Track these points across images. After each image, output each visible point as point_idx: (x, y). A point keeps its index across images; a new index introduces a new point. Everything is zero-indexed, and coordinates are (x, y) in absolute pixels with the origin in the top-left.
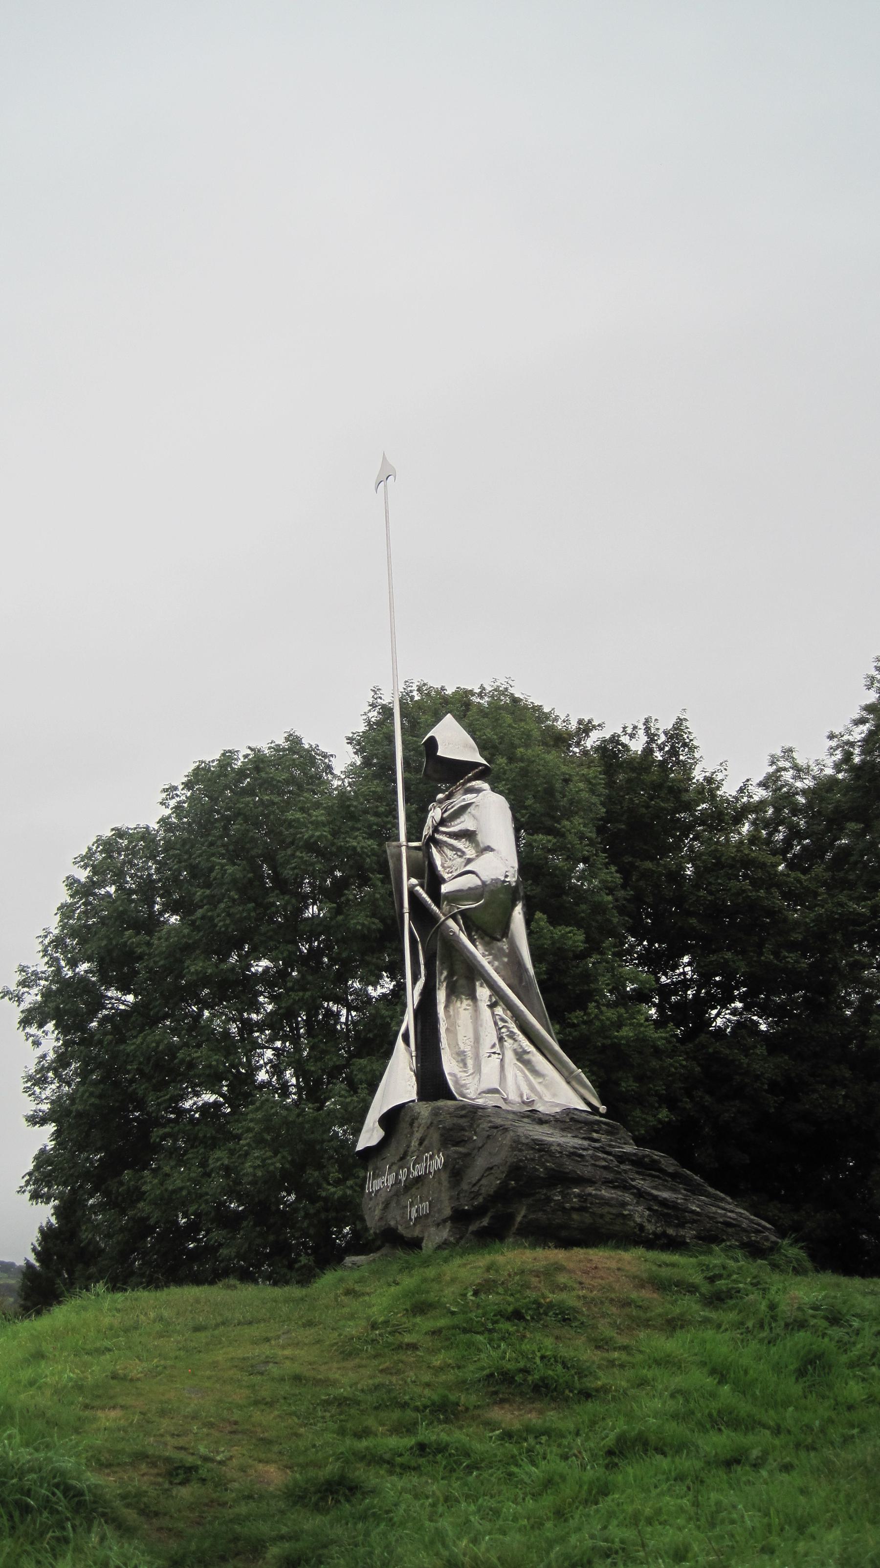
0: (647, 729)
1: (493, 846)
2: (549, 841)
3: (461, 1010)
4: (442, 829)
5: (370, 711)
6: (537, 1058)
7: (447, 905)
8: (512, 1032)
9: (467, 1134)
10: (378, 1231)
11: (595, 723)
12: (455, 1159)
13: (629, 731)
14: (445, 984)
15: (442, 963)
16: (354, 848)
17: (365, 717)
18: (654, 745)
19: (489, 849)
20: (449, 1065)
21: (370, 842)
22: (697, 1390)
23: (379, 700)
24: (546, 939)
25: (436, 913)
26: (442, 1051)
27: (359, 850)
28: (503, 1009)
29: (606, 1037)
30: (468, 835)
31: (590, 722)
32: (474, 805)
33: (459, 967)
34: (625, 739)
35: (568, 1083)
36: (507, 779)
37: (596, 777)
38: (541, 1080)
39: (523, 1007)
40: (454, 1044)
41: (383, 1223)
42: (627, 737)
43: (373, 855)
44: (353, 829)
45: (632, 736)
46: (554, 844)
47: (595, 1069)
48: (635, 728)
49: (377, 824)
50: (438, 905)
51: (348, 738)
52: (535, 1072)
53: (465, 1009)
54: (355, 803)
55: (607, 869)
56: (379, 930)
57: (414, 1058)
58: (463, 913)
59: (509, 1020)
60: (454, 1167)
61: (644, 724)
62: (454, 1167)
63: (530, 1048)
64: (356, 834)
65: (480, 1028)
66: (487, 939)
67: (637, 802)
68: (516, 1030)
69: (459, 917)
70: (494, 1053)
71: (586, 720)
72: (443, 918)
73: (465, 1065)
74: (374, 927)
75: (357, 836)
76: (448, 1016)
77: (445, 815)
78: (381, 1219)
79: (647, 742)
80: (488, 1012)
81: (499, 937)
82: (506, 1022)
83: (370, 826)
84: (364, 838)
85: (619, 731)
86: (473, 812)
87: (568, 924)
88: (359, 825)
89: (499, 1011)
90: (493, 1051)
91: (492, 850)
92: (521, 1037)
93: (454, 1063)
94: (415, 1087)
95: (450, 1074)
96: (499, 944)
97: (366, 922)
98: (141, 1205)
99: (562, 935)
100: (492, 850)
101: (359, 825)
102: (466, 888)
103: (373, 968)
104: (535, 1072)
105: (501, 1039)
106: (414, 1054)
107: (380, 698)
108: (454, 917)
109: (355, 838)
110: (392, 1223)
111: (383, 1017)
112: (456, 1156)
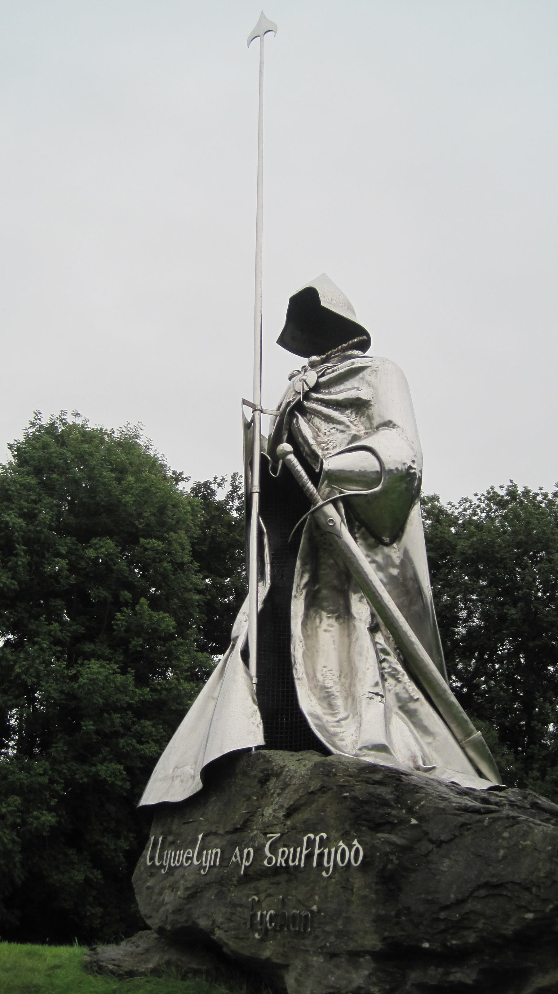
0: (233, 482)
1: (395, 420)
2: (159, 546)
4: (314, 395)
5: (30, 428)
6: (425, 709)
7: (328, 486)
8: (395, 669)
9: (394, 812)
10: (168, 927)
11: (184, 476)
12: (387, 854)
13: (219, 481)
14: (304, 592)
15: (303, 565)
16: (7, 523)
17: (26, 431)
18: (235, 495)
19: (388, 424)
20: (308, 703)
21: (20, 520)
23: (38, 421)
24: (146, 620)
25: (312, 495)
26: (297, 683)
27: (11, 524)
29: (179, 704)
30: (358, 406)
31: (181, 474)
32: (368, 370)
33: (328, 574)
34: (214, 487)
35: (463, 748)
36: (132, 494)
37: (197, 506)
38: (430, 740)
39: (414, 638)
40: (312, 676)
41: (182, 918)
42: (216, 485)
43: (21, 531)
44: (7, 507)
45: (220, 485)
46: (162, 548)
47: (166, 726)
48: (223, 479)
49: (27, 508)
50: (316, 483)
51: (9, 445)
52: (424, 730)
53: (325, 631)
54: (13, 488)
55: (196, 575)
56: (15, 590)
58: (346, 500)
59: (392, 653)
60: (385, 867)
61: (232, 477)
62: (385, 867)
63: (417, 694)
64: (10, 512)
65: (356, 658)
66: (372, 540)
67: (220, 532)
68: (399, 667)
69: (341, 505)
70: (377, 694)
71: (178, 472)
72: (321, 503)
73: (331, 706)
74: (13, 587)
75: (11, 514)
76: (306, 636)
77: (322, 380)
78: (178, 911)
79: (231, 491)
81: (387, 540)
82: (388, 654)
83: (21, 509)
84: (16, 516)
85: (211, 480)
86: (368, 378)
87: (165, 612)
88: (13, 506)
89: (380, 638)
90: (376, 690)
91: (394, 426)
92: (406, 678)
93: (315, 701)
94: (261, 727)
95: (311, 715)
96: (386, 550)
97: (7, 582)
99: (160, 618)
100: (394, 426)
101: (13, 506)
102: (347, 469)
103: (5, 620)
104: (424, 730)
105: (382, 676)
106: (255, 680)
107: (40, 419)
108: (334, 502)
109: (9, 515)
110: (203, 923)
111: (8, 661)
112: (388, 849)
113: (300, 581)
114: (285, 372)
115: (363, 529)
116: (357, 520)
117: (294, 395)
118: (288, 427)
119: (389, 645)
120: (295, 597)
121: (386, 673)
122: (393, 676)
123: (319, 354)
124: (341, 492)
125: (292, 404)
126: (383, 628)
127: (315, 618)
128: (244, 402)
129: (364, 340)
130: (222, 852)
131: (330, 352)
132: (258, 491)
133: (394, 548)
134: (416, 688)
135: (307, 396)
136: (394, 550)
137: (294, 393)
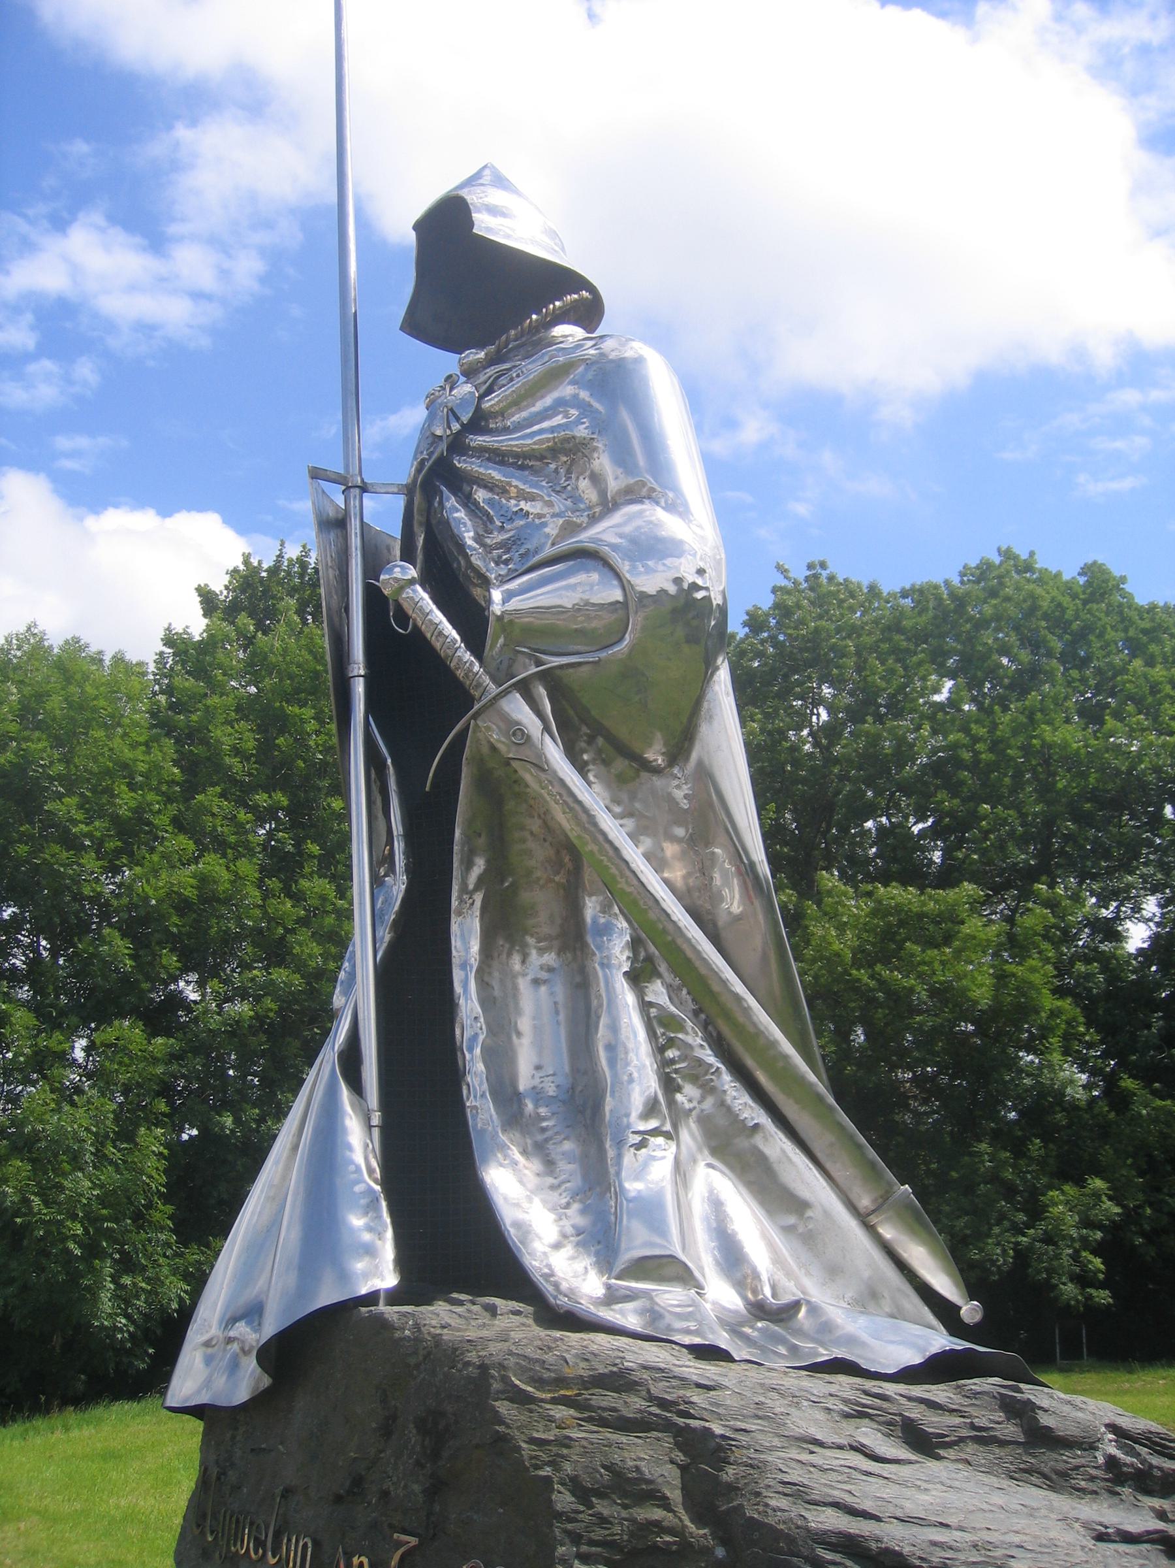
3: (523, 984)
4: (479, 440)
14: (478, 898)
22: (377, 1267)
28: (669, 987)
57: (376, 1132)
66: (621, 764)
69: (541, 691)
80: (629, 998)
89: (658, 992)
92: (727, 1080)
96: (658, 782)
98: (627, 563)
105: (669, 1085)
106: (376, 1119)
108: (525, 689)
113: (468, 875)
114: (407, 398)
115: (600, 741)
116: (583, 721)
117: (431, 444)
118: (423, 520)
119: (680, 1004)
120: (459, 914)
121: (676, 1071)
122: (694, 1079)
123: (480, 345)
124: (539, 663)
125: (428, 465)
126: (663, 968)
127: (509, 954)
128: (316, 474)
129: (582, 300)
130: (317, 1544)
131: (504, 338)
132: (362, 672)
133: (676, 777)
134: (750, 1102)
135: (457, 445)
136: (676, 782)
137: (430, 440)
